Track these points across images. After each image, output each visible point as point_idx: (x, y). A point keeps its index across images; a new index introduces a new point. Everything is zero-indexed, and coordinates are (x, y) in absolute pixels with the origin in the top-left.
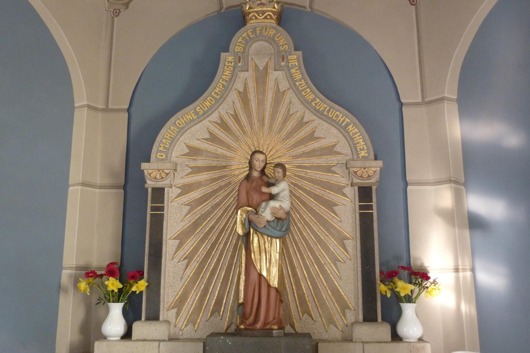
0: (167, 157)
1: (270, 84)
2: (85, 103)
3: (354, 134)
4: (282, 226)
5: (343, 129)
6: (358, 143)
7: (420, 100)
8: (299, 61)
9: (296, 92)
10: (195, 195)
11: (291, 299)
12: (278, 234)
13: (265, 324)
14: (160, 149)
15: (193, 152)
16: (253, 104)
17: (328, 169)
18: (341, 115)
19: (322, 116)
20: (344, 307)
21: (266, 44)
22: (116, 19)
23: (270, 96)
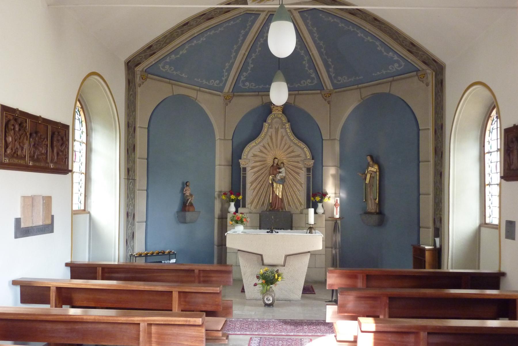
4: (283, 181)
10: (256, 169)
11: (285, 201)
15: (255, 156)
16: (274, 140)
18: (302, 145)
20: (301, 204)
23: (279, 137)
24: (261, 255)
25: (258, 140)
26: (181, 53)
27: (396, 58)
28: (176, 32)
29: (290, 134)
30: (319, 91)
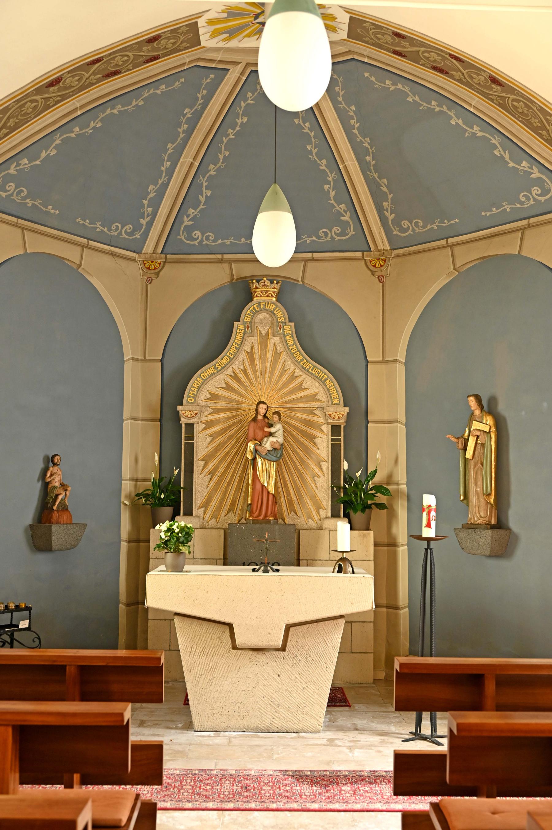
0: (195, 401)
1: (270, 347)
2: (131, 356)
3: (330, 387)
5: (323, 382)
6: (333, 393)
7: (381, 359)
8: (291, 330)
9: (289, 354)
11: (283, 501)
12: (275, 459)
13: (266, 516)
14: (190, 395)
15: (214, 397)
16: (257, 362)
17: (311, 412)
19: (307, 373)
20: (318, 508)
21: (267, 315)
22: (149, 285)
23: (270, 355)
24: (288, 628)
25: (222, 360)
26: (43, 155)
27: (536, 174)
28: (32, 101)
29: (295, 347)
30: (359, 254)
